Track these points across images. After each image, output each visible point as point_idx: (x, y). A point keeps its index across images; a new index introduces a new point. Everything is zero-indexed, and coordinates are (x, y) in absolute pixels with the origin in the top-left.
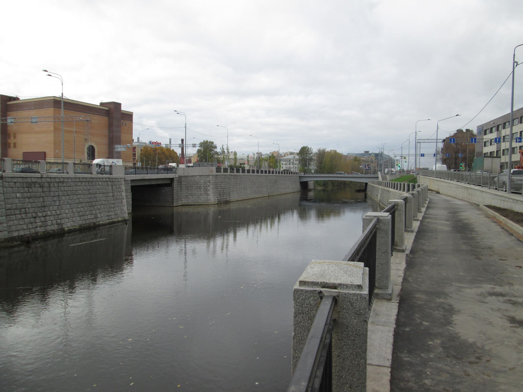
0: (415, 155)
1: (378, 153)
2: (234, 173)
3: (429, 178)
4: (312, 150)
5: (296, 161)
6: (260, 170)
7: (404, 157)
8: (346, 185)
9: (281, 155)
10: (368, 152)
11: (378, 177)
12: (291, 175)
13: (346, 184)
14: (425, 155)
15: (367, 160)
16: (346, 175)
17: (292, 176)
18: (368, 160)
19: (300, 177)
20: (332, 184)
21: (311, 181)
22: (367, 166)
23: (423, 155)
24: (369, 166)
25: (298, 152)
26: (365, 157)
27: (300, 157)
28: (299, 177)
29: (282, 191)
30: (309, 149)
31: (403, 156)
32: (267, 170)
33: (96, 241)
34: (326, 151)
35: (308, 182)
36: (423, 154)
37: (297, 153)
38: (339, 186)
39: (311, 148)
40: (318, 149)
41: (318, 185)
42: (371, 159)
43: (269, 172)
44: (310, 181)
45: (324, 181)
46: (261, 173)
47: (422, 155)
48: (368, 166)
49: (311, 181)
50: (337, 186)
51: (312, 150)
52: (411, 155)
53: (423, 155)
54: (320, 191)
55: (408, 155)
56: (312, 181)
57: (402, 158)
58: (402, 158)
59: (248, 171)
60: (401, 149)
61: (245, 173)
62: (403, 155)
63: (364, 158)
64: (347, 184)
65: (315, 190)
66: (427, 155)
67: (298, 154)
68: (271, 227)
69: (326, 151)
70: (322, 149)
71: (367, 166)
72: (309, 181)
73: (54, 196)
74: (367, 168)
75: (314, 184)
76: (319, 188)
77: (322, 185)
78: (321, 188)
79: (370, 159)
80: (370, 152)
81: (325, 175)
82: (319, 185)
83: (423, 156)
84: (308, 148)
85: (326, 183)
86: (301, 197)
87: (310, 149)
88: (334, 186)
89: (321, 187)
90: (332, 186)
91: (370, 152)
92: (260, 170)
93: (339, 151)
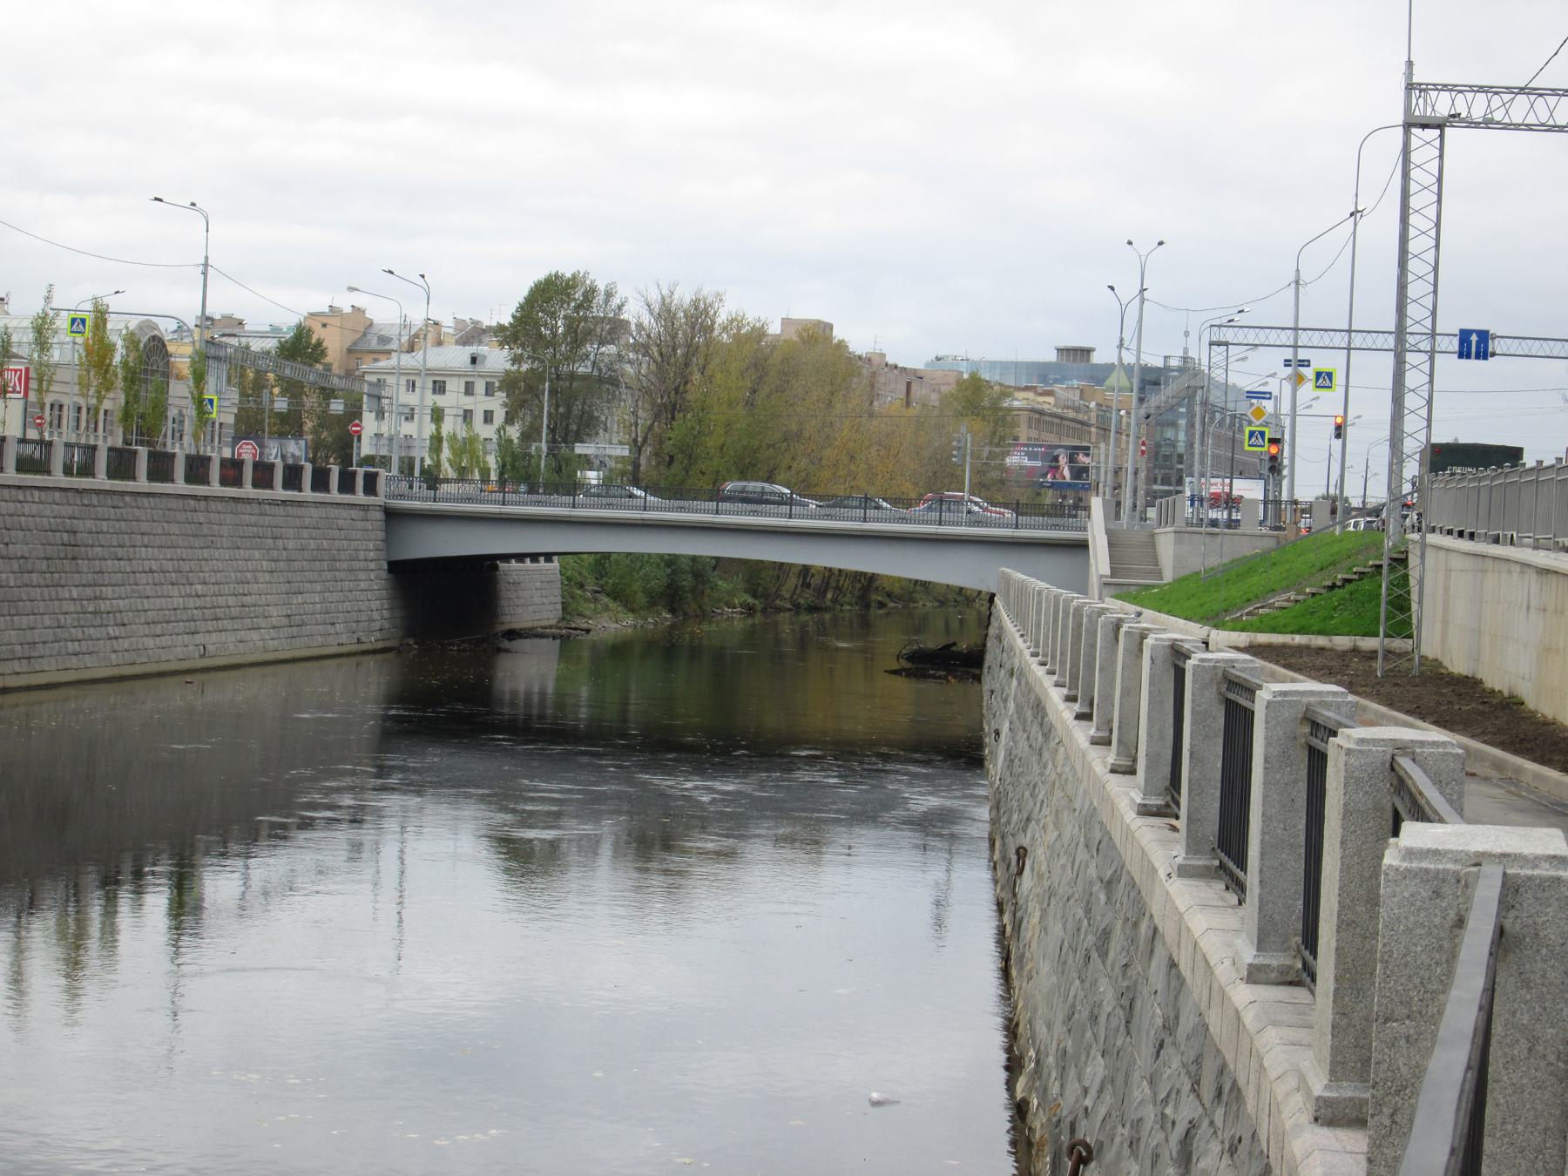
0: (1391, 342)
1: (1159, 363)
2: (49, 473)
3: (1544, 572)
4: (620, 308)
5: (489, 392)
6: (143, 452)
7: (1319, 375)
8: (882, 605)
9: (384, 340)
10: (1086, 352)
11: (1082, 546)
12: (279, 493)
13: (875, 597)
14: (1495, 346)
15: (1071, 414)
16: (810, 517)
17: (300, 503)
18: (1080, 417)
19: (393, 516)
20: (755, 596)
21: (535, 557)
22: (1063, 460)
23: (1475, 345)
24: (1083, 459)
25: (506, 320)
26: (1057, 388)
27: (516, 360)
28: (380, 515)
29: (150, 643)
30: (600, 298)
31: (1305, 363)
32: (177, 450)
33: (1151, 684)
34: (722, 318)
35: (502, 565)
36: (1484, 336)
37: (501, 328)
38: (812, 609)
39: (609, 295)
40: (654, 297)
41: (605, 599)
42: (1098, 405)
43: (263, 475)
44: (520, 557)
45: (671, 561)
46: (154, 476)
47: (1474, 338)
48: (1072, 459)
49: (535, 557)
50: (797, 607)
51: (620, 308)
52: (1369, 341)
53: (1475, 345)
54: (619, 650)
55: (1340, 340)
56: (548, 557)
57: (1298, 380)
58: (1298, 380)
59: (197, 469)
60: (1291, 291)
61: (326, 489)
62: (1303, 354)
63: (1050, 400)
64: (889, 595)
65: (566, 638)
66: (1514, 346)
67: (506, 336)
68: (73, 964)
69: (722, 318)
70: (684, 296)
71: (1063, 460)
72: (506, 558)
73: (94, 613)
74: (1066, 473)
75: (571, 583)
76: (612, 624)
77: (648, 593)
78: (629, 620)
79: (1093, 405)
80: (1097, 358)
81: (681, 509)
82: (619, 595)
83: (1483, 354)
84: (591, 292)
85: (687, 582)
86: (399, 696)
87: (607, 301)
88: (764, 611)
89: (633, 611)
90: (750, 610)
91: (1097, 358)
92: (143, 452)
93: (857, 336)
